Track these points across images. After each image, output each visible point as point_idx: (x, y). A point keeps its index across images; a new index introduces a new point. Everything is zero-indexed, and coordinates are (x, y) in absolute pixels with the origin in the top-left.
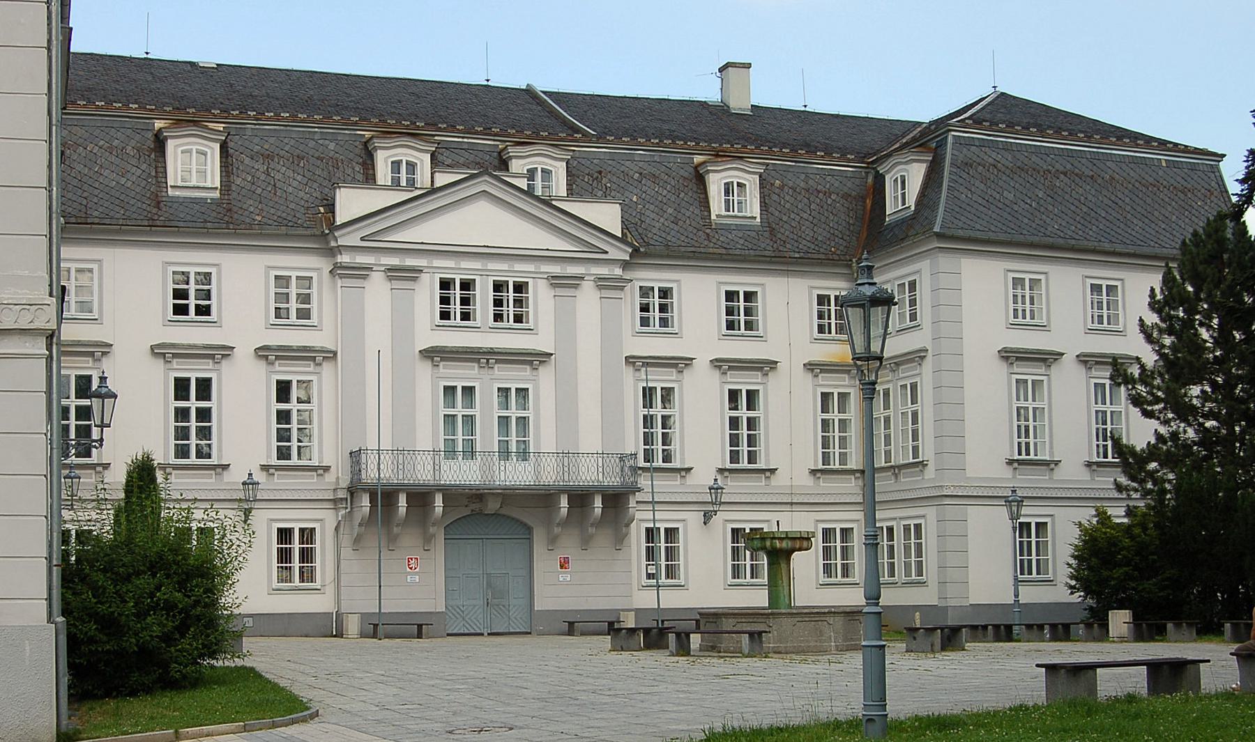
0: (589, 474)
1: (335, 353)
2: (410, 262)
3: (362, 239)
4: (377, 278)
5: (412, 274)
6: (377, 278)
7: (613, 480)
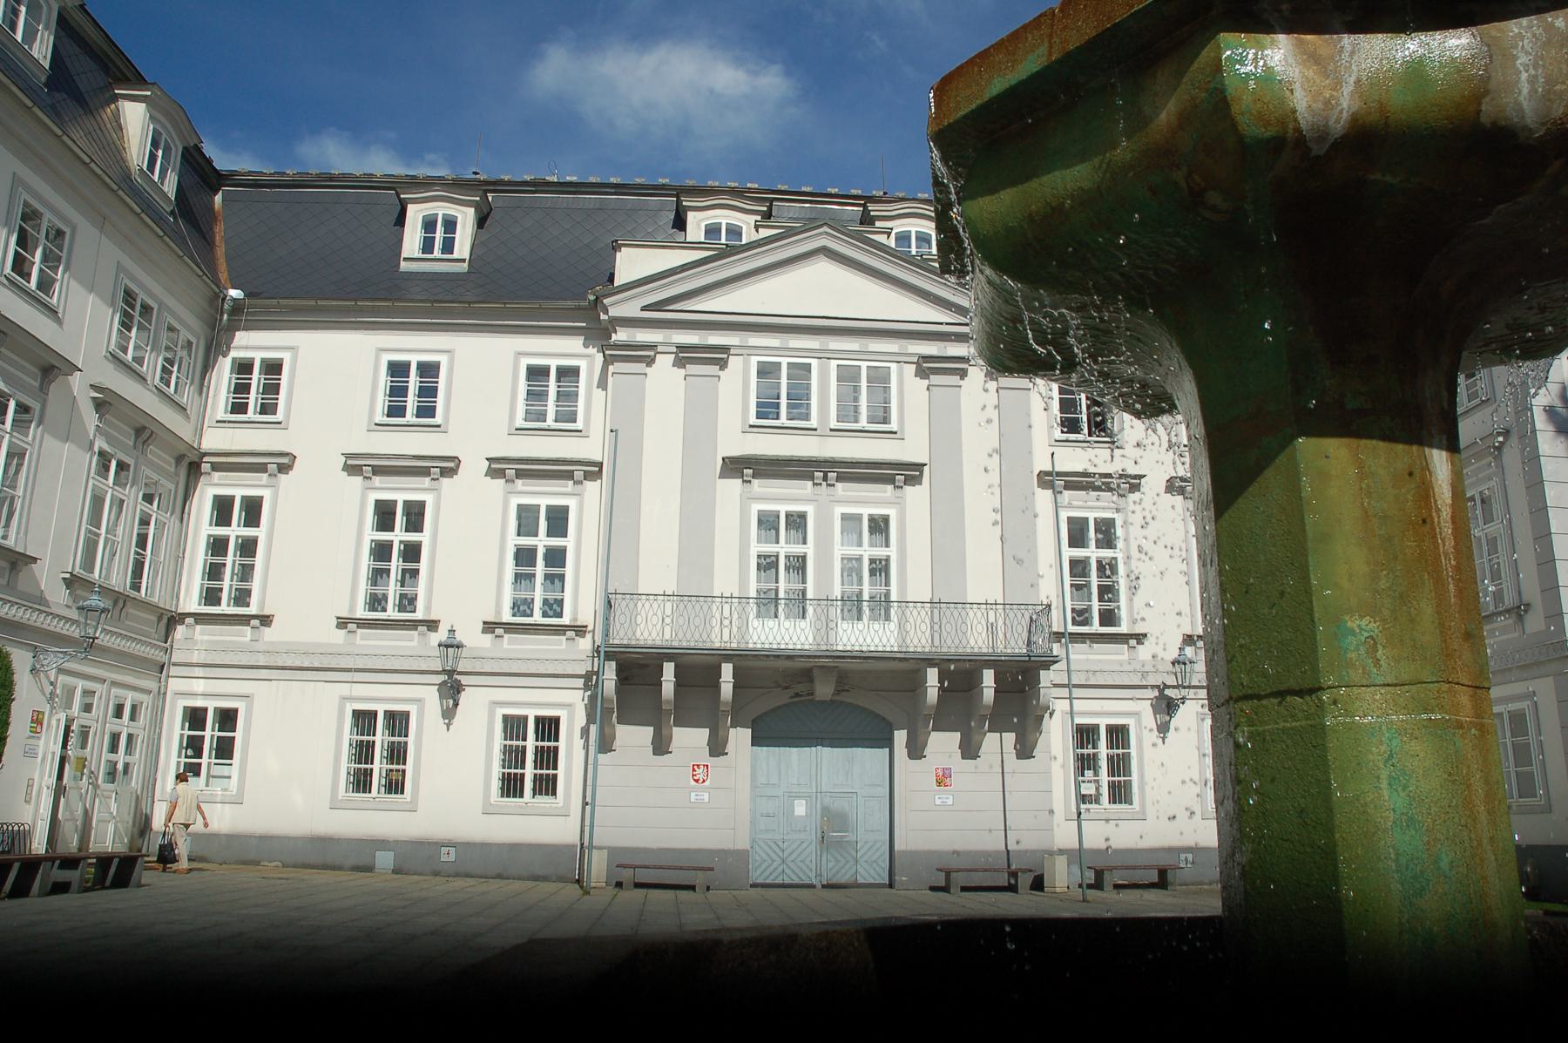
0: (976, 637)
1: (600, 465)
2: (715, 339)
3: (644, 309)
4: (664, 361)
5: (718, 357)
6: (664, 361)
7: (1013, 645)
